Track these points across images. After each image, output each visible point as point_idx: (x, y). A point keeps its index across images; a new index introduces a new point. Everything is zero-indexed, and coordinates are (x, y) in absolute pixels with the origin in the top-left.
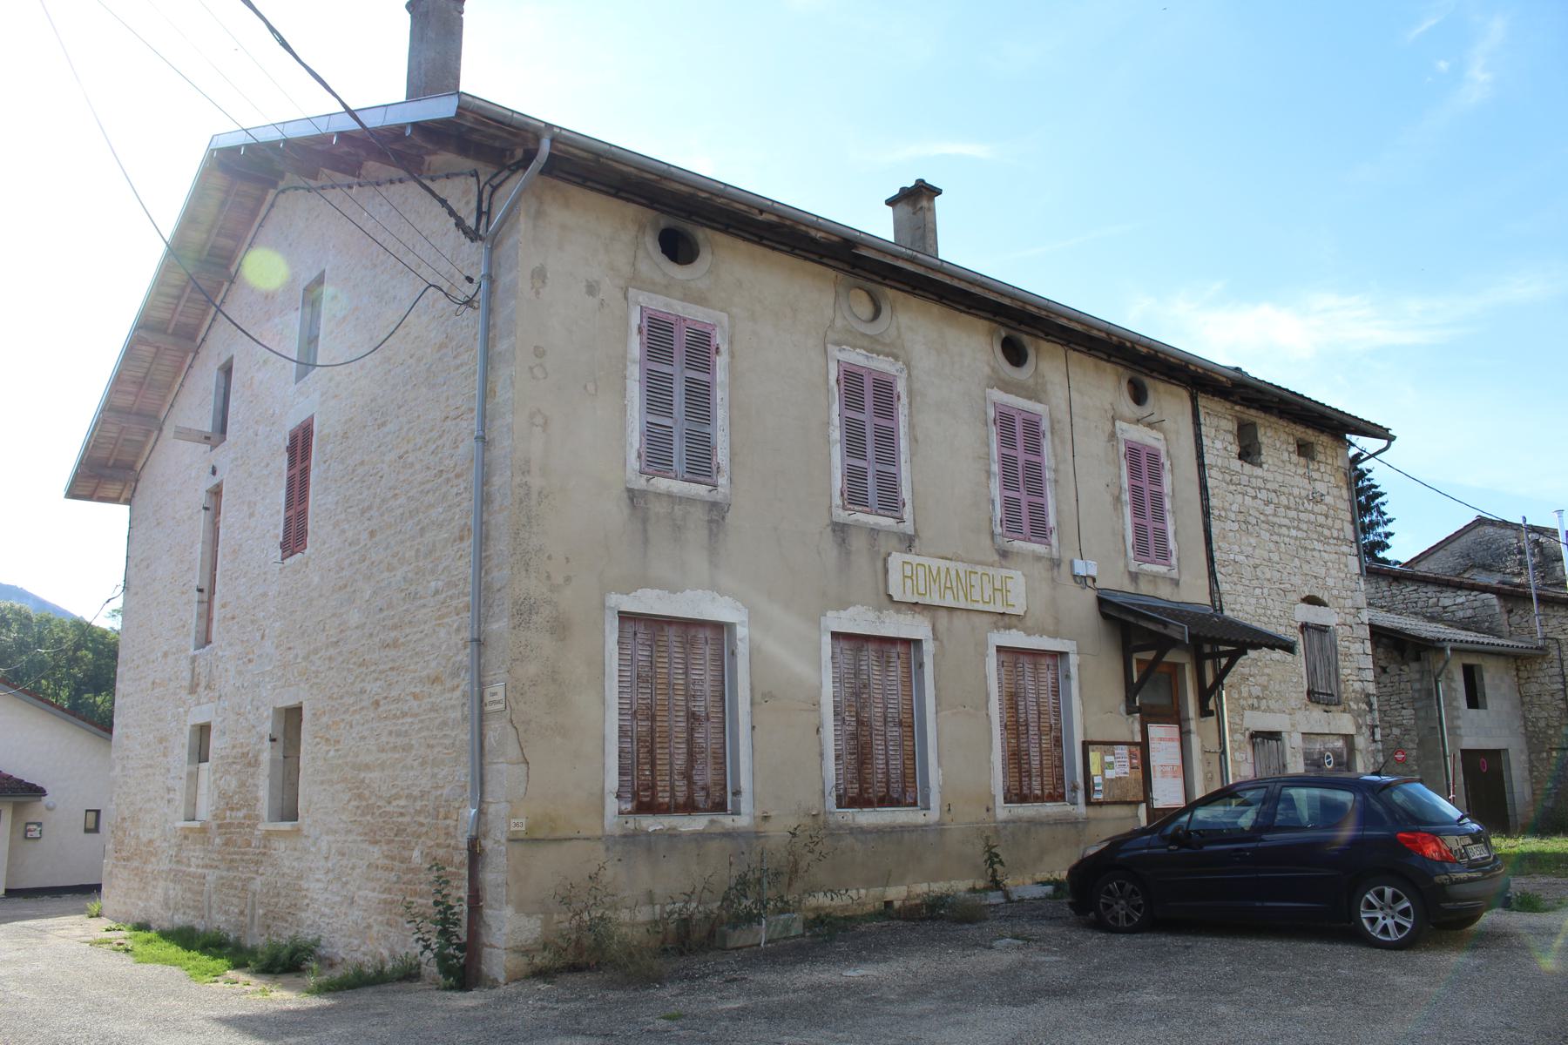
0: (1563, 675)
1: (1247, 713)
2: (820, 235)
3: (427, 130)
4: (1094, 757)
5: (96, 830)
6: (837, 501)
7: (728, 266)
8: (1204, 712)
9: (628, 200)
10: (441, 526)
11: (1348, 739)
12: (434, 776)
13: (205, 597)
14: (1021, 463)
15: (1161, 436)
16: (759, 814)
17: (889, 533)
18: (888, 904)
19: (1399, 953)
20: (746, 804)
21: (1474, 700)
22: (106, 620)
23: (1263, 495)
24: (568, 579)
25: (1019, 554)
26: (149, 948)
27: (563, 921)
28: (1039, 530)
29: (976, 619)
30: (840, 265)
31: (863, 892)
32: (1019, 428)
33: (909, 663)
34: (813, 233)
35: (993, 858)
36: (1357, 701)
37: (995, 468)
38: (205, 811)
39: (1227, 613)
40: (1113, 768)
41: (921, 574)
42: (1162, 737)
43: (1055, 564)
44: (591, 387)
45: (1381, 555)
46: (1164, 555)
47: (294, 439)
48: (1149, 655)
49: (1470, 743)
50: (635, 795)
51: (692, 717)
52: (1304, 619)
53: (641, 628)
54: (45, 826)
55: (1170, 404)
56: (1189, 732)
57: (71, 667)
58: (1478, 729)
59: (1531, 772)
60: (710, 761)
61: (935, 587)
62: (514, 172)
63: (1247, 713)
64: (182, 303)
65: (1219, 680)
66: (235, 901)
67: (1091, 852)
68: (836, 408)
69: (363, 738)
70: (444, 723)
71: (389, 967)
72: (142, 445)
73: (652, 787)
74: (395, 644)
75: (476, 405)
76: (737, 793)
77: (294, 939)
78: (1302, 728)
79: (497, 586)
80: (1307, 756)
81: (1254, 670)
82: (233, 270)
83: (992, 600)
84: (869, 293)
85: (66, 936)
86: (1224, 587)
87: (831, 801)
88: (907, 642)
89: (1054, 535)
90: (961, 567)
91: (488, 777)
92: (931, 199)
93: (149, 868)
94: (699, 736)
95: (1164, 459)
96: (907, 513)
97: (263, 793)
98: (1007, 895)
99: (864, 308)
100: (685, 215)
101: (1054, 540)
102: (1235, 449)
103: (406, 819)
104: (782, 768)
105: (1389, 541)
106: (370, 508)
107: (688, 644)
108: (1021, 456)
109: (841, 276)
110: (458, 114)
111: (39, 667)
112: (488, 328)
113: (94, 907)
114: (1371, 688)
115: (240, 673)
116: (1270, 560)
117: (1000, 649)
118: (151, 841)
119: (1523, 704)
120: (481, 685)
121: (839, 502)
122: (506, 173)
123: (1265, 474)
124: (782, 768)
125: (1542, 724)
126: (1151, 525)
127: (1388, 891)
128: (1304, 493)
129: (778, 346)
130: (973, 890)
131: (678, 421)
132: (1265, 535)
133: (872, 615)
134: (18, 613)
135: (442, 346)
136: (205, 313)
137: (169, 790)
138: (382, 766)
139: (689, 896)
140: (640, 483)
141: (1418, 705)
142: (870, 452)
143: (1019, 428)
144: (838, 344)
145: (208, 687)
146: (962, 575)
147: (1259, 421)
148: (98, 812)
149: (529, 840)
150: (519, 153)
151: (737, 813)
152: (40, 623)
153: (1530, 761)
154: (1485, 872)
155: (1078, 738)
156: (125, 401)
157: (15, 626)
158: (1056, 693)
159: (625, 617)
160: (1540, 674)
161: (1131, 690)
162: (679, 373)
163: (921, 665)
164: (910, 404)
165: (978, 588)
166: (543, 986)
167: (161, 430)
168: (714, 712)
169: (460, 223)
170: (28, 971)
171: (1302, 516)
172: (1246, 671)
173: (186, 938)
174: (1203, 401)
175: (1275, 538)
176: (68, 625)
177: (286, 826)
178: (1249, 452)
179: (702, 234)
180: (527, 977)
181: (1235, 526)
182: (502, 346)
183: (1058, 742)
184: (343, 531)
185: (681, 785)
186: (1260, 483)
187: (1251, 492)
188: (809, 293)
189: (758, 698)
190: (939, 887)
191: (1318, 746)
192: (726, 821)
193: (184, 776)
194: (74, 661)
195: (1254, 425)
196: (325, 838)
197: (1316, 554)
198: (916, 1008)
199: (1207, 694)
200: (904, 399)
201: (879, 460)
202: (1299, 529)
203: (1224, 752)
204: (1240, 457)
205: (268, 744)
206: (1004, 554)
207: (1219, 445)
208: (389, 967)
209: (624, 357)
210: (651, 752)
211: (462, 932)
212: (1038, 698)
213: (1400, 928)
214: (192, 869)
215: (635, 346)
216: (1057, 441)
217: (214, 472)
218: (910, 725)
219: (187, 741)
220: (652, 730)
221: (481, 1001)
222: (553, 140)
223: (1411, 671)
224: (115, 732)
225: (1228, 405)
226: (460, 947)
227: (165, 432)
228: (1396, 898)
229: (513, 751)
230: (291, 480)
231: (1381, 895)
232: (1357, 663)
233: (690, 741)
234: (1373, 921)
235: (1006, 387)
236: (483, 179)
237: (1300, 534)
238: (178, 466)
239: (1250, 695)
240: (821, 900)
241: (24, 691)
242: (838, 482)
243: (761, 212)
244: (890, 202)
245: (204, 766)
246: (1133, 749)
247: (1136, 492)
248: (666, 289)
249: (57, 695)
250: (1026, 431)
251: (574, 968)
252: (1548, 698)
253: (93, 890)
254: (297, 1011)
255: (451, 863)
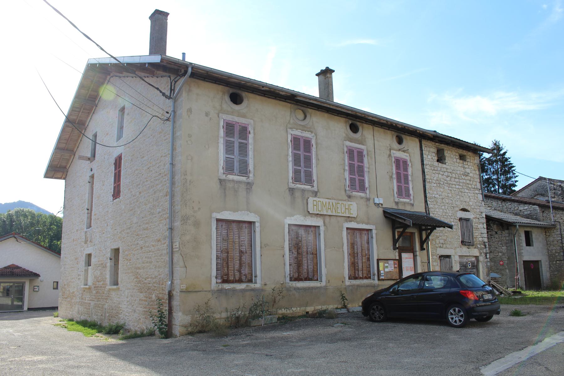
0: (561, 235)
1: (438, 249)
2: (283, 93)
3: (153, 65)
4: (381, 264)
5: (57, 288)
6: (291, 181)
7: (253, 106)
8: (422, 249)
9: (219, 84)
10: (160, 191)
11: (477, 257)
12: (159, 271)
13: (89, 212)
14: (356, 166)
15: (408, 155)
16: (263, 283)
17: (308, 191)
18: (307, 313)
19: (457, 329)
20: (259, 280)
21: (529, 243)
22: (61, 215)
23: (446, 174)
24: (199, 209)
25: (355, 197)
26: (73, 327)
27: (197, 317)
28: (362, 188)
29: (339, 219)
30: (292, 102)
31: (298, 308)
32: (355, 154)
33: (316, 234)
34: (281, 93)
35: (343, 298)
36: (480, 244)
37: (347, 168)
38: (90, 283)
39: (431, 215)
40: (388, 268)
41: (320, 204)
42: (407, 258)
43: (368, 199)
44: (207, 146)
45: (513, 189)
46: (408, 196)
47: (116, 160)
48: (401, 230)
49: (526, 258)
50: (222, 277)
51: (241, 252)
52: (461, 217)
53: (224, 224)
54: (40, 287)
55: (412, 144)
56: (416, 256)
57: (49, 232)
58: (529, 254)
59: (550, 268)
60: (247, 266)
61: (324, 209)
62: (181, 77)
63: (438, 249)
64: (80, 113)
65: (427, 237)
66: (100, 311)
67: (369, 295)
68: (290, 150)
69: (138, 259)
70: (162, 255)
71: (145, 332)
72: (68, 160)
73: (228, 275)
74: (147, 229)
75: (170, 152)
76: (256, 277)
77: (117, 323)
78: (458, 254)
79: (177, 211)
80: (461, 263)
81: (441, 234)
82: (97, 102)
83: (345, 212)
84: (302, 111)
85: (46, 324)
86: (430, 206)
87: (288, 279)
88: (315, 227)
89: (368, 190)
90: (334, 201)
91: (174, 272)
92: (331, 74)
93: (73, 301)
94: (243, 258)
95: (409, 163)
96: (315, 184)
97: (108, 276)
98: (348, 310)
99: (301, 115)
100: (238, 90)
101: (368, 192)
102: (436, 158)
103: (151, 285)
104: (271, 268)
105: (516, 184)
106: (139, 184)
107: (240, 229)
108: (356, 163)
109: (292, 105)
110: (161, 61)
111: (39, 232)
112: (174, 128)
113: (56, 313)
114: (486, 240)
115: (100, 237)
116: (448, 196)
117: (347, 229)
118: (73, 292)
119: (547, 244)
120: (172, 242)
121: (291, 181)
122: (179, 77)
123: (447, 167)
124: (271, 268)
125: (554, 251)
126: (403, 185)
127: (457, 309)
128: (461, 173)
129: (271, 130)
130: (337, 308)
131: (236, 157)
132: (446, 188)
133: (302, 218)
134: (30, 212)
135: (160, 133)
136: (79, 136)
137: (79, 275)
138: (144, 268)
139: (238, 310)
140: (224, 177)
141: (508, 245)
142: (302, 164)
143: (355, 154)
144: (291, 128)
145: (91, 241)
146: (334, 204)
147: (445, 148)
148: (57, 282)
149: (187, 291)
150: (183, 71)
151: (374, 280)
152: (38, 216)
153: (550, 265)
154: (492, 303)
155: (375, 258)
156: (63, 146)
157: (30, 217)
158: (368, 243)
159: (218, 220)
160: (553, 234)
161: (395, 241)
162: (236, 141)
163: (320, 234)
164: (317, 147)
165: (340, 208)
166: (190, 337)
167: (75, 155)
168: (249, 251)
169: (164, 94)
170: (34, 333)
171: (461, 181)
172: (438, 234)
173: (84, 324)
174: (424, 142)
175: (450, 189)
176: (47, 215)
177: (115, 287)
178: (441, 159)
179: (244, 94)
180: (186, 335)
181: (435, 185)
182: (178, 134)
183: (368, 259)
184: (131, 192)
185: (237, 274)
186: (445, 170)
187: (441, 173)
188: (282, 112)
189: (263, 245)
190: (324, 307)
191: (465, 260)
192: (252, 285)
193: (83, 270)
194: (50, 229)
195: (443, 150)
196: (126, 291)
197: (466, 194)
198: (300, 344)
199: (422, 243)
200: (314, 146)
201: (305, 167)
202: (459, 185)
203: (429, 262)
204: (438, 161)
205: (109, 260)
206: (349, 197)
207: (429, 157)
208: (145, 332)
209: (218, 136)
210: (227, 263)
211: (166, 320)
212: (361, 245)
213: (460, 321)
214: (86, 301)
215: (222, 132)
216: (369, 158)
217: (91, 170)
218: (315, 254)
219: (84, 259)
220: (228, 257)
221: (241, 362)
222: (192, 68)
223: (505, 233)
224: (62, 256)
225: (433, 143)
226: (166, 325)
227: (76, 156)
228: (459, 311)
229: (181, 264)
230: (115, 174)
231: (455, 310)
232: (480, 231)
233: (240, 260)
234: (452, 318)
235: (351, 140)
236: (172, 78)
237: (460, 187)
238: (80, 168)
239: (440, 243)
240: (283, 311)
241: (32, 242)
242: (291, 174)
243: (263, 87)
244: (317, 75)
245: (90, 267)
246: (395, 261)
247: (398, 174)
248: (232, 113)
249: (44, 241)
250: (358, 155)
251: (200, 332)
252: (556, 242)
253: (55, 308)
254: (114, 345)
255: (164, 299)
